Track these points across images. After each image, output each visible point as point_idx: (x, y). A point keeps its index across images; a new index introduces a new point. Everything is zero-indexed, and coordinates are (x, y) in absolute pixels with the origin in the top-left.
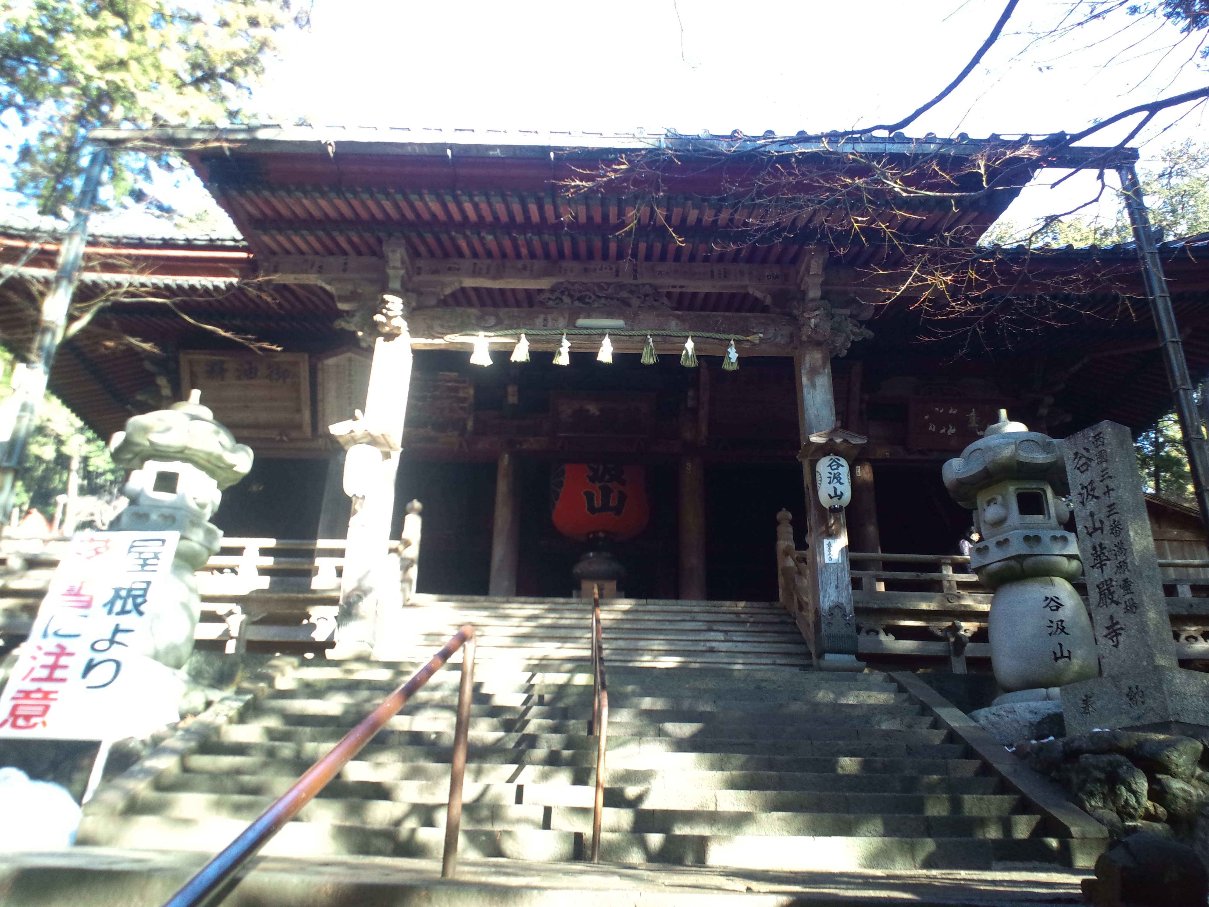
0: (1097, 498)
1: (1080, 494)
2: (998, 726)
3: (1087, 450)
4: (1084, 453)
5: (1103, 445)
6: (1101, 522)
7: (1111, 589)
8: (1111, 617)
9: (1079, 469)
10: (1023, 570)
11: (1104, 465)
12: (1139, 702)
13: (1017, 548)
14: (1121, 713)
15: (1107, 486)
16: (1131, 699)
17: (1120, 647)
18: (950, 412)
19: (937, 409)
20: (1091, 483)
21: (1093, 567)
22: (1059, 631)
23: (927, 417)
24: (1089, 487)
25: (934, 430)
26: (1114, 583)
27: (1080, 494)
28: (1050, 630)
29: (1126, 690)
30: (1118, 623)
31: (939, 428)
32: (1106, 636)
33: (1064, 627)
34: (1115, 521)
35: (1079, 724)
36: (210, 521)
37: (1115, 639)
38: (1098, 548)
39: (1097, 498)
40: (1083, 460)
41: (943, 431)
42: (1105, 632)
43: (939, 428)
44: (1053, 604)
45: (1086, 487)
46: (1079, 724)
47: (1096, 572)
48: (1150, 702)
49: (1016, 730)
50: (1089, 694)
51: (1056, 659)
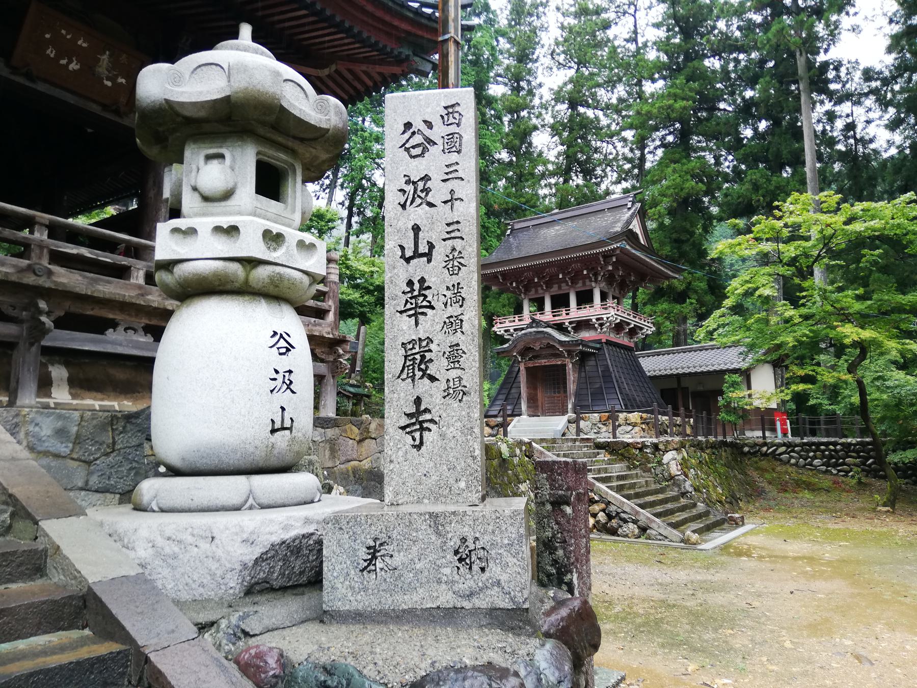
0: (431, 205)
1: (402, 191)
2: (175, 563)
3: (429, 125)
4: (423, 127)
5: (458, 125)
6: (431, 246)
7: (428, 356)
8: (418, 401)
9: (407, 150)
10: (247, 281)
11: (454, 157)
12: (475, 568)
13: (251, 244)
14: (439, 582)
15: (452, 192)
16: (461, 560)
17: (423, 448)
18: (80, 43)
19: (63, 32)
20: (426, 178)
21: (401, 312)
22: (285, 387)
23: (47, 36)
24: (421, 185)
25: (52, 56)
26: (433, 346)
27: (402, 191)
28: (273, 384)
29: (455, 542)
30: (427, 411)
31: (59, 56)
32: (403, 428)
33: (291, 382)
34: (454, 249)
35: (352, 588)
36: (564, 366)
37: (417, 435)
38: (417, 286)
39: (431, 205)
40: (418, 139)
41: (63, 62)
42: (404, 421)
43: (59, 56)
44: (282, 343)
45: (414, 183)
46: (352, 588)
47: (406, 322)
48: (494, 570)
49: (212, 575)
50: (383, 537)
51: (273, 431)
